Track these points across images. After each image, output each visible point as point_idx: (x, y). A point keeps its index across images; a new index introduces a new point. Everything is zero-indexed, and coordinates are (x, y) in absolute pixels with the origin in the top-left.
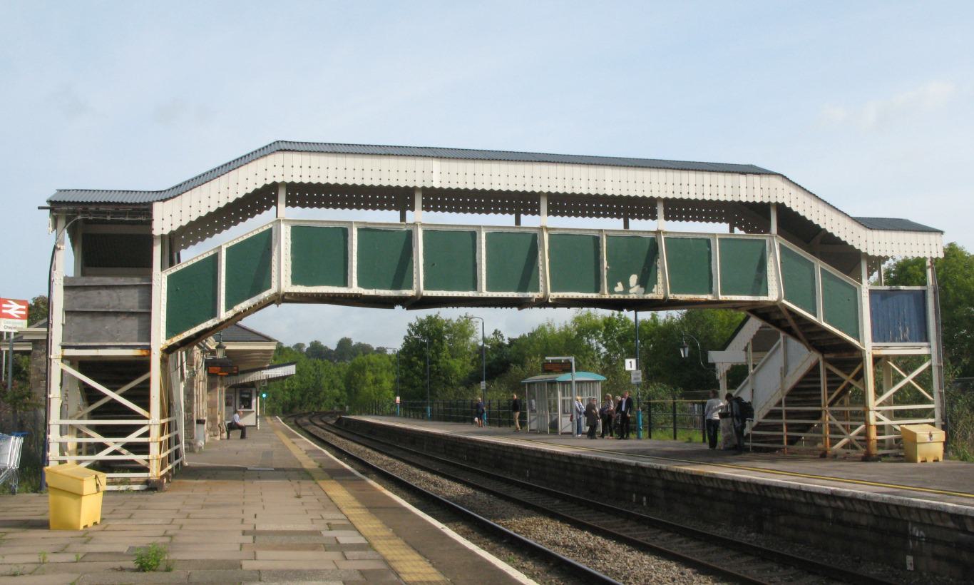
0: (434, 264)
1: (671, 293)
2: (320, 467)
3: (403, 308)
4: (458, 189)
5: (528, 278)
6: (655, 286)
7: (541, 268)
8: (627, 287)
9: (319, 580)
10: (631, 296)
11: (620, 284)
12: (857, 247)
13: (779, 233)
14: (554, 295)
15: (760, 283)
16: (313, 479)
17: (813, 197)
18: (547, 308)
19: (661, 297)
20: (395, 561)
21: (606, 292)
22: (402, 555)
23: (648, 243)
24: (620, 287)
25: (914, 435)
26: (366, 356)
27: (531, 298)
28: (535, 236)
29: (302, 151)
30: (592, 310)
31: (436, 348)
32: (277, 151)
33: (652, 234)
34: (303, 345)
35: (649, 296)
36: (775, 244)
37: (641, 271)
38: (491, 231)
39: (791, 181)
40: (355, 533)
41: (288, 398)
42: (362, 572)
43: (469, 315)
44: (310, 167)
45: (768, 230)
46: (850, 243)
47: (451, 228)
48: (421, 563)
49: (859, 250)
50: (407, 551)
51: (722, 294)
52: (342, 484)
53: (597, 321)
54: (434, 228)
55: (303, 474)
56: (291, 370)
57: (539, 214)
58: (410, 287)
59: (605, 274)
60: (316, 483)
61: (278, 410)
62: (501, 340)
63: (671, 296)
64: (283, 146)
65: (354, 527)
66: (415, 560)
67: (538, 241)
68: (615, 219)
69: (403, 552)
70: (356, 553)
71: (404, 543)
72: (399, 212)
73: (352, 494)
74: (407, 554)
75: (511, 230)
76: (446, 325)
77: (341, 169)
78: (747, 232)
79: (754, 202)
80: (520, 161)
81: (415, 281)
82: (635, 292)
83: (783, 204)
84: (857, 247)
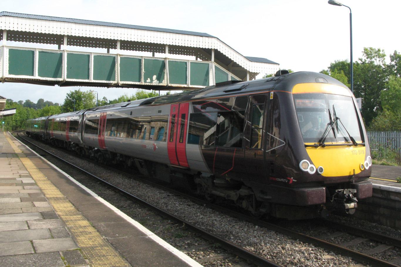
0: (71, 68)
1: (170, 83)
2: (22, 152)
3: (59, 86)
4: (128, 41)
5: (111, 75)
6: (164, 80)
7: (116, 71)
8: (152, 80)
9: (10, 197)
10: (153, 84)
11: (149, 79)
12: (245, 68)
13: (215, 61)
14: (121, 83)
15: (206, 81)
16: (18, 157)
17: (229, 47)
18: (134, 88)
19: (165, 85)
20: (45, 190)
21: (143, 82)
22: (48, 187)
23: (161, 63)
24: (149, 80)
25: (26, 134)
26: (49, 107)
27: (111, 83)
28: (114, 58)
29: (14, 17)
30: (144, 90)
31: (78, 104)
32: (3, 16)
33: (163, 59)
34: (22, 101)
35: (161, 84)
36: (213, 65)
37: (158, 74)
38: (96, 55)
39: (220, 40)
40: (31, 179)
41: (14, 124)
42: (29, 194)
43: (92, 90)
44: (18, 24)
45: (211, 60)
46: (243, 67)
47: (27, 49)
48: (56, 190)
49: (246, 70)
50: (51, 186)
51: (190, 85)
52: (30, 159)
53: (146, 94)
54: (72, 53)
55: (15, 155)
56: (14, 111)
57: (63, 45)
58: (61, 77)
59: (143, 75)
60: (19, 159)
61: (10, 129)
62: (106, 101)
63: (170, 85)
64: (5, 14)
65: (31, 176)
66: (53, 189)
67: (116, 60)
68: (149, 52)
69: (49, 186)
70: (29, 187)
71: (51, 183)
72: (58, 45)
73: (34, 163)
74: (51, 187)
75: (105, 55)
76: (83, 95)
77: (20, 24)
78: (203, 60)
79: (205, 48)
80: (165, 32)
81: (63, 74)
82: (155, 83)
83: (217, 50)
84: (245, 68)
